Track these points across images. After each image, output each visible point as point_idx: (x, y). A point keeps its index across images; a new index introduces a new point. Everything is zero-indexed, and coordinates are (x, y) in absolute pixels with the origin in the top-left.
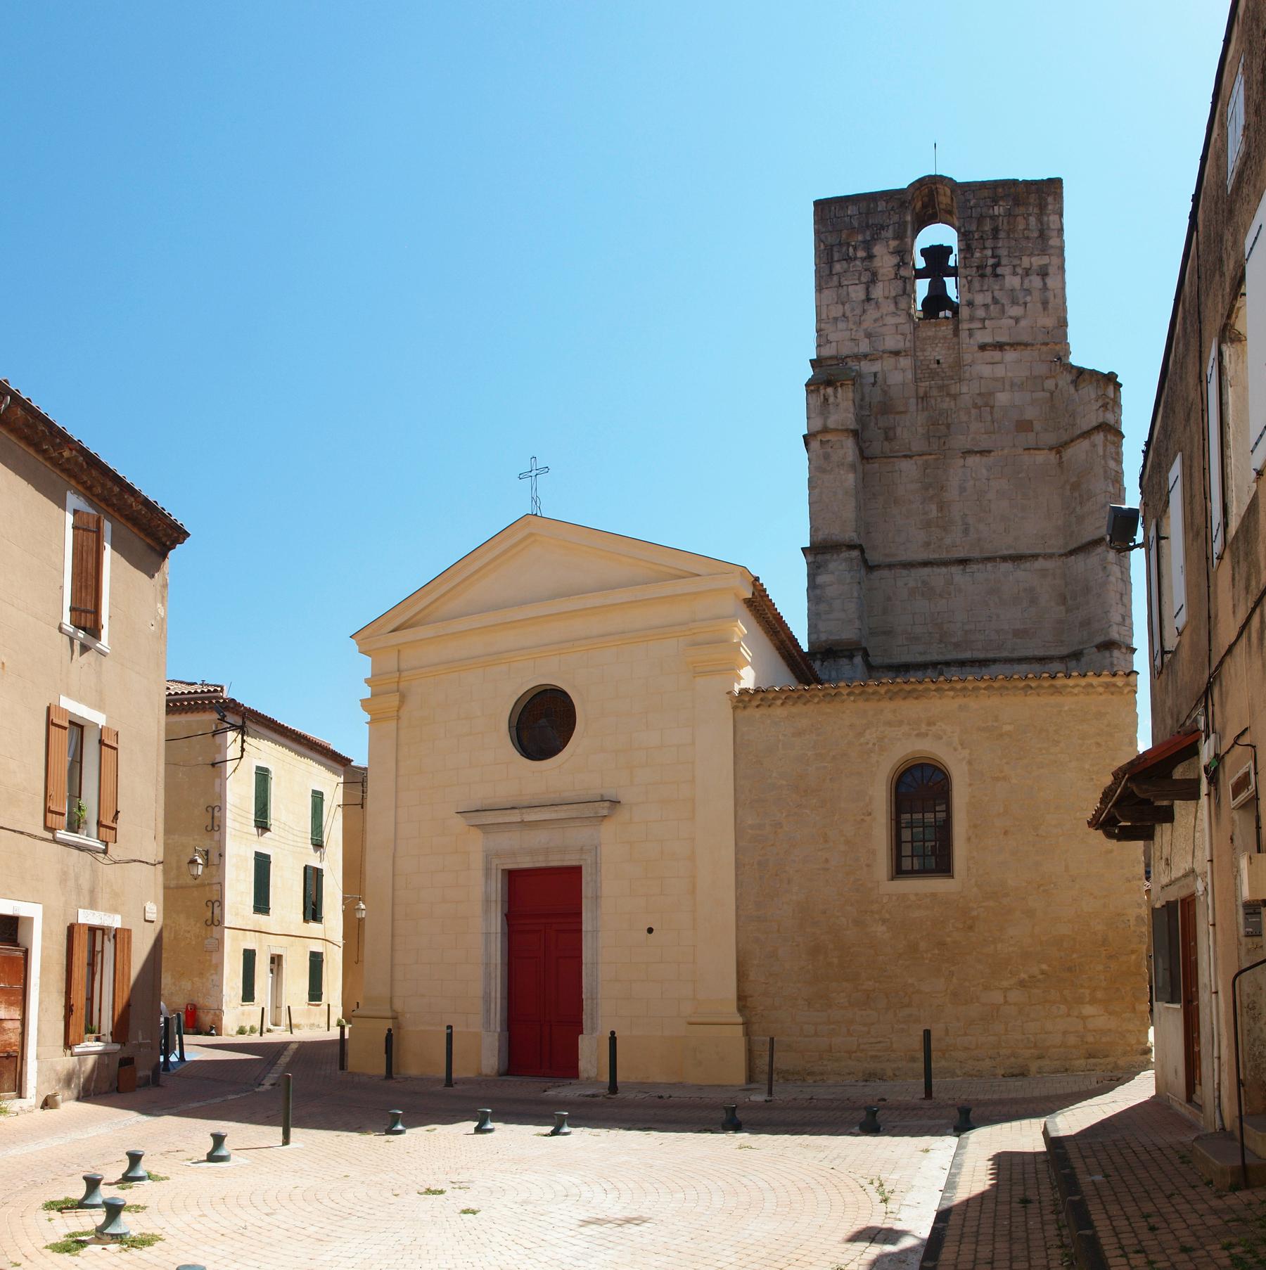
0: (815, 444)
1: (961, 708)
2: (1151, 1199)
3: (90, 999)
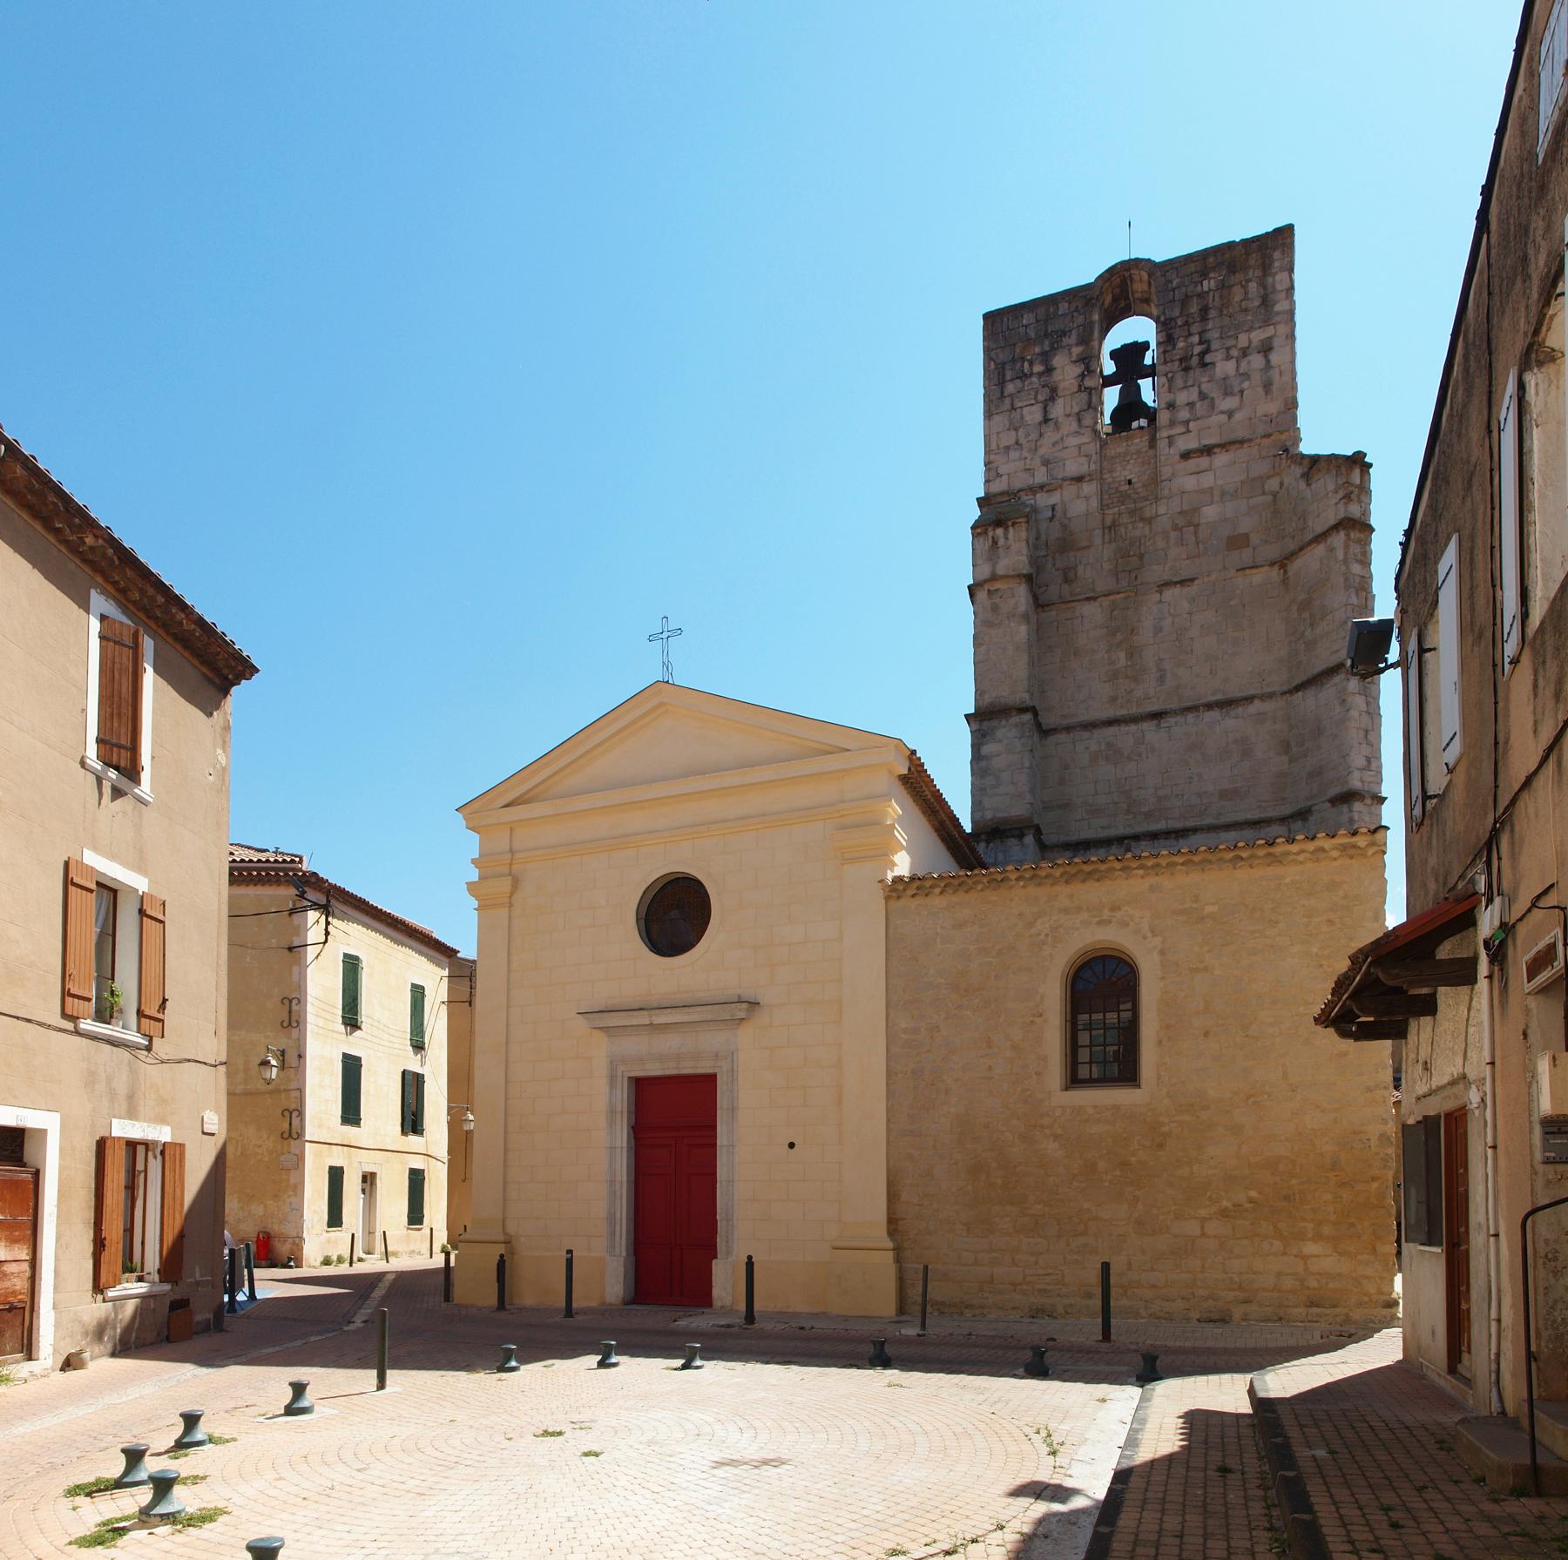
0: (982, 595)
1: (1152, 889)
2: (1394, 1489)
3: (129, 1231)
